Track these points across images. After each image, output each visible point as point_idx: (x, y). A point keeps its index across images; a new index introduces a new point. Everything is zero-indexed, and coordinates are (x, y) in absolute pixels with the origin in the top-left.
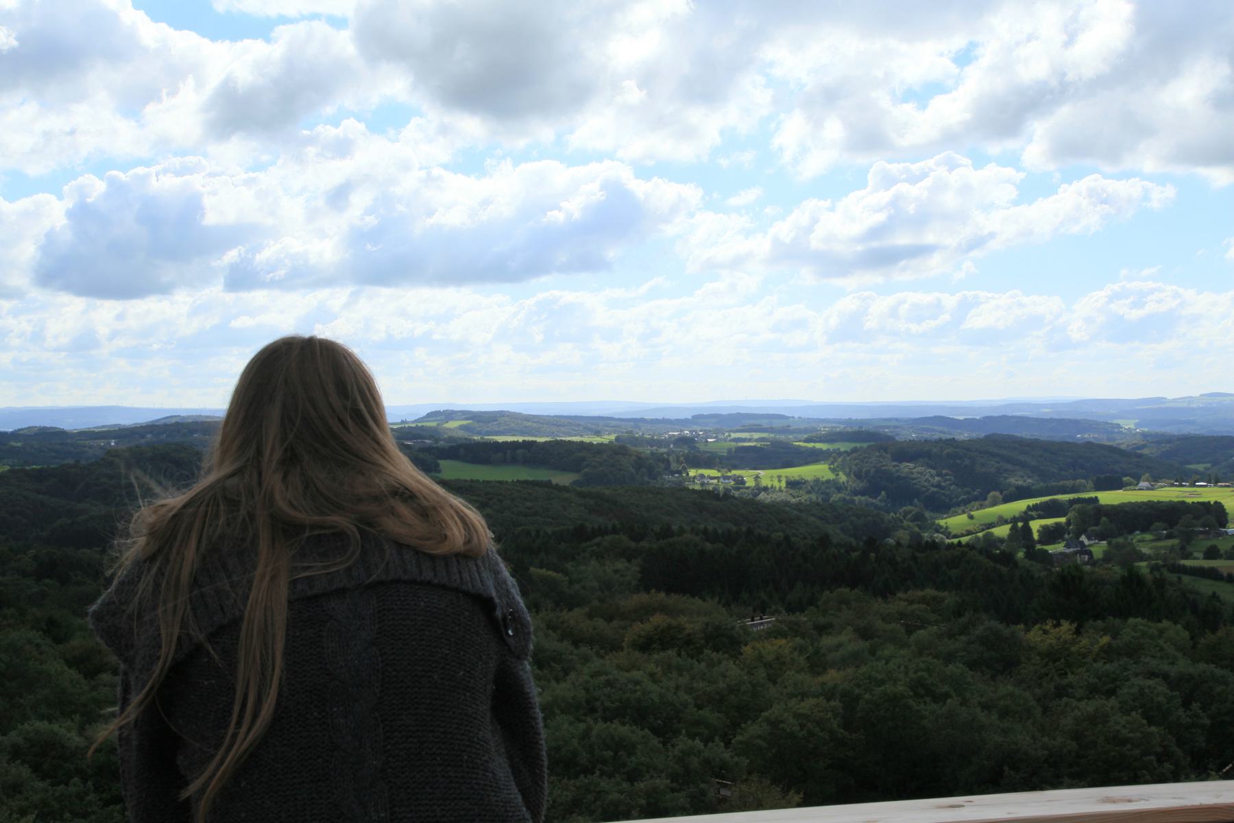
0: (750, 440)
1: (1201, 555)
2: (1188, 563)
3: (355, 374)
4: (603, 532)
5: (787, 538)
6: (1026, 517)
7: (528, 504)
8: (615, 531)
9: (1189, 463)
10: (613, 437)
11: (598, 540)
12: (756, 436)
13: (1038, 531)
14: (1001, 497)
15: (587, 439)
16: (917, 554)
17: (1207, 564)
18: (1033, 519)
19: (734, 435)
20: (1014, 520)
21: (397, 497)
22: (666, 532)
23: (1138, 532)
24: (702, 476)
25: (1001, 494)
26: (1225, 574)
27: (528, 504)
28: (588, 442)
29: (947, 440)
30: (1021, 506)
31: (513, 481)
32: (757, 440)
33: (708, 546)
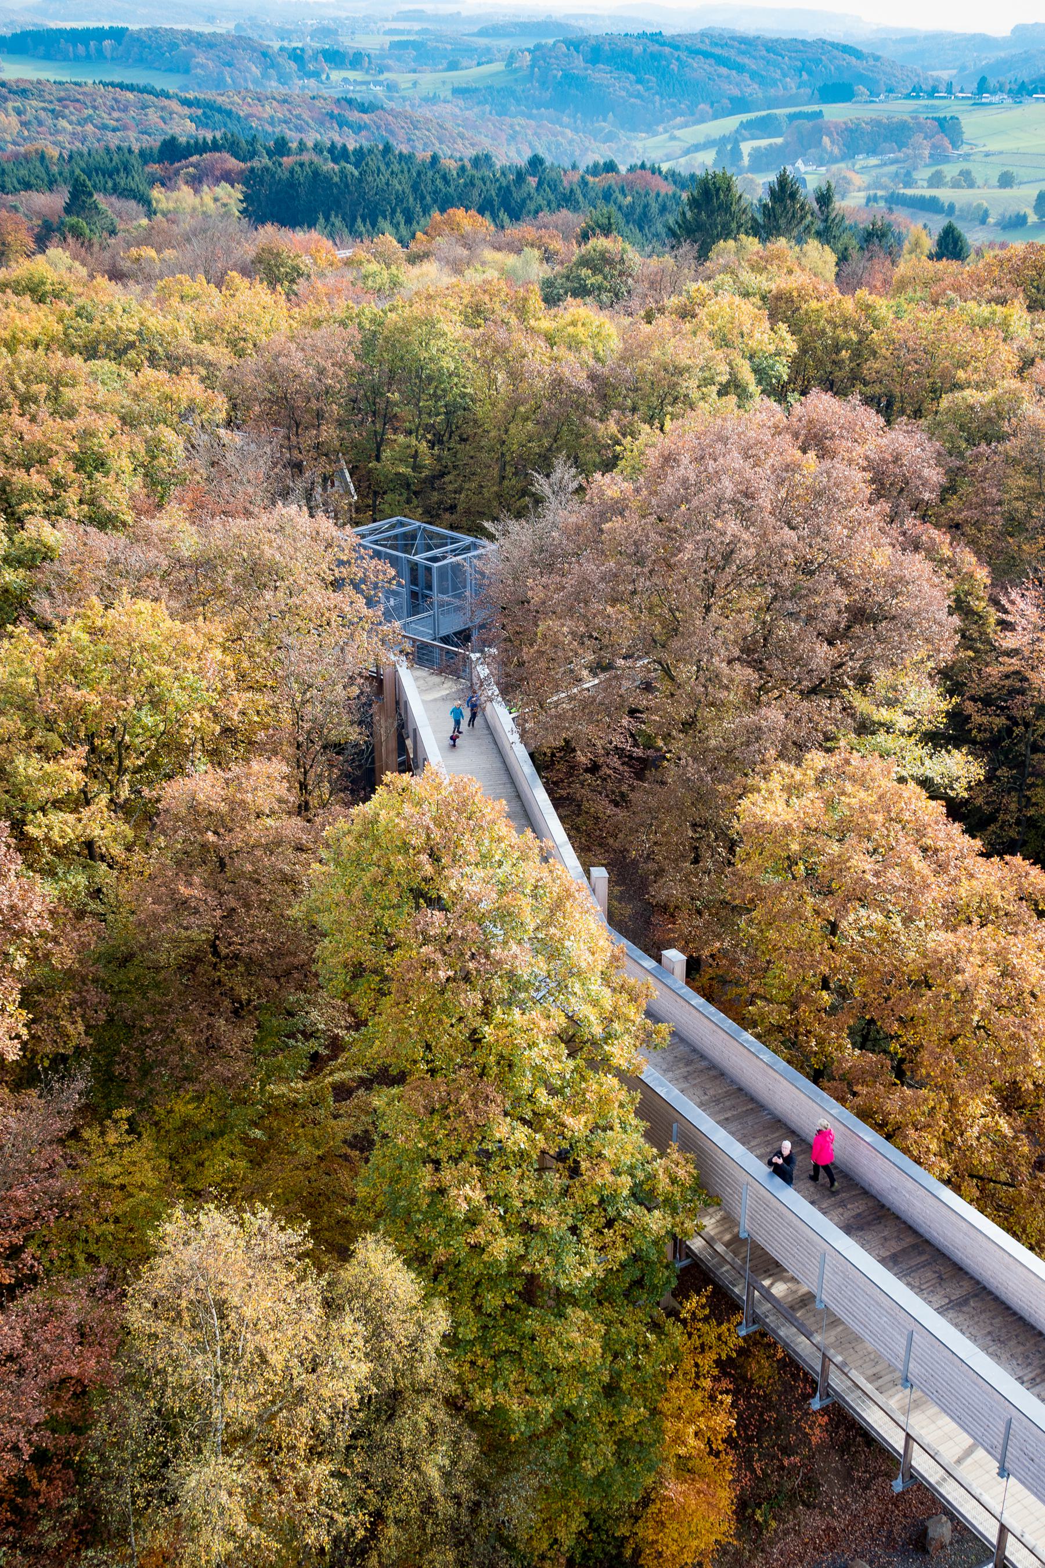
0: (409, 32)
1: (925, 184)
2: (909, 192)
3: (397, 703)
4: (201, 148)
5: (435, 159)
6: (736, 138)
7: (116, 115)
8: (215, 147)
9: (934, 69)
10: (231, 26)
11: (194, 159)
12: (417, 26)
13: (750, 155)
14: (710, 111)
15: (196, 28)
16: (590, 179)
17: (928, 193)
18: (745, 139)
19: (389, 26)
20: (723, 141)
21: (375, 1086)
22: (281, 147)
23: (861, 157)
24: (345, 80)
25: (712, 107)
26: (946, 205)
27: (116, 115)
28: (107, 27)
29: (652, 34)
30: (730, 124)
31: (467, 210)
32: (417, 33)
33: (329, 166)
